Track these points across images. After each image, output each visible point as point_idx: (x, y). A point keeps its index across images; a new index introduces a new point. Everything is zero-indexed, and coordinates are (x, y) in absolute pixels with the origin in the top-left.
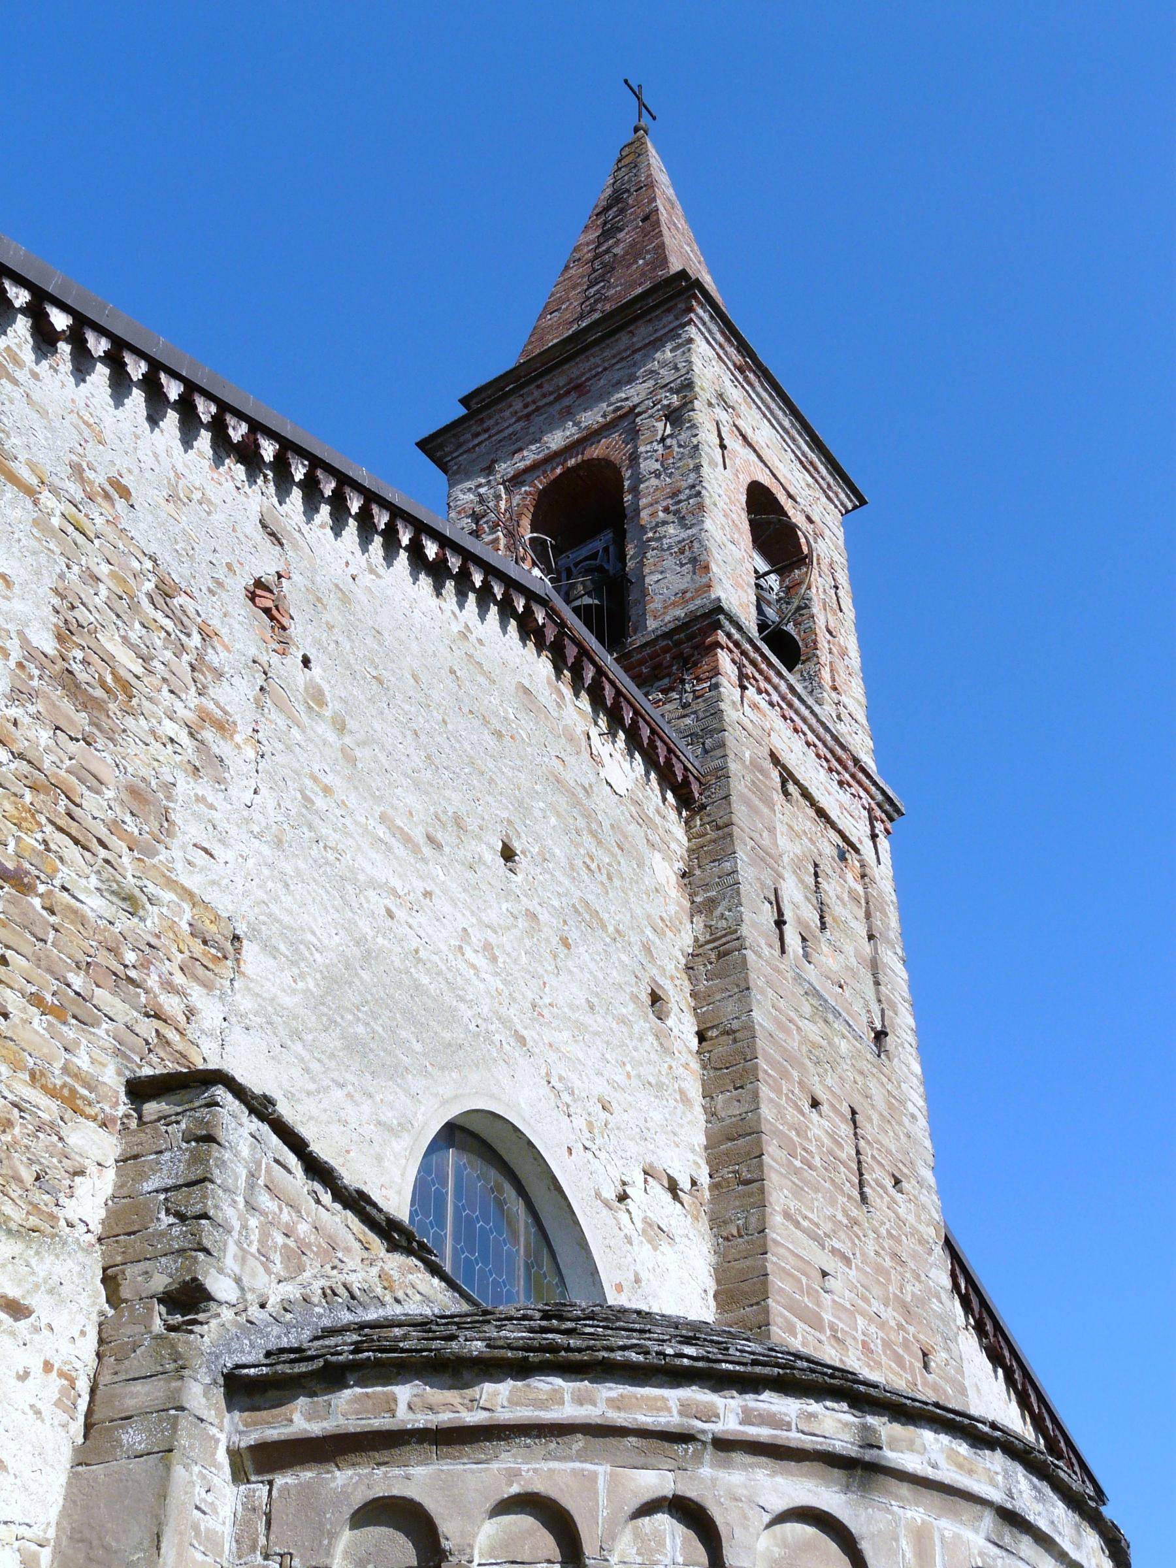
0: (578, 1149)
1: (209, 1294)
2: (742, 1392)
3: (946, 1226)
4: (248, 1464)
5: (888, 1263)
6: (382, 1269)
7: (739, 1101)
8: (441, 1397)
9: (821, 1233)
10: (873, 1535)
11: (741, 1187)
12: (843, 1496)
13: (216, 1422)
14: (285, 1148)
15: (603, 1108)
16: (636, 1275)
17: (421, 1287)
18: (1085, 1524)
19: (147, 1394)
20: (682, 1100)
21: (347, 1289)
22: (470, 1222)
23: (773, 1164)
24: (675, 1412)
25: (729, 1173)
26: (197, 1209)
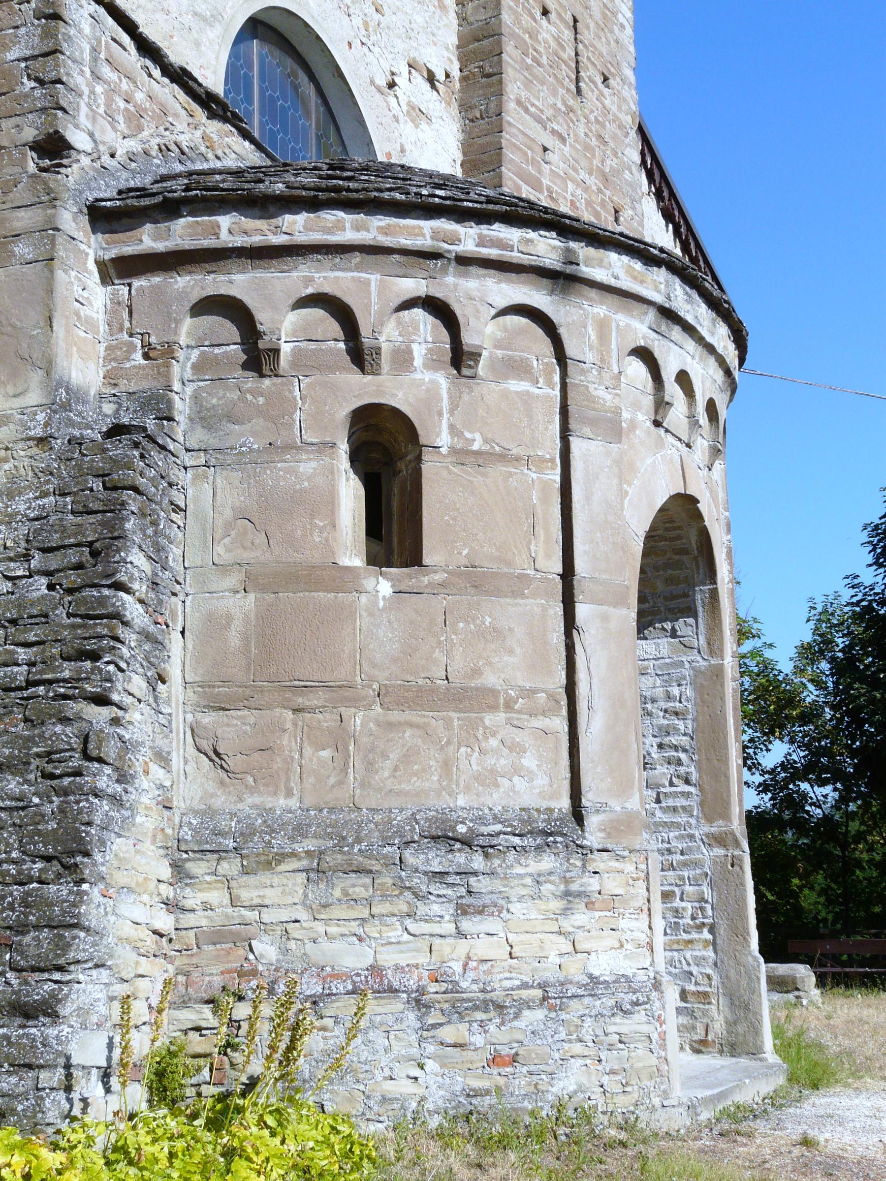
0: (356, 44)
1: (69, 144)
2: (479, 223)
3: (640, 116)
4: (112, 271)
5: (594, 142)
6: (204, 132)
7: (485, 8)
8: (253, 224)
9: (544, 117)
10: (569, 324)
11: (484, 80)
12: (549, 297)
13: (85, 240)
14: (120, 29)
15: (377, 10)
16: (402, 146)
17: (236, 148)
18: (719, 319)
19: (30, 219)
20: (439, 6)
21: (178, 146)
22: (272, 100)
23: (510, 61)
24: (428, 237)
25: (475, 68)
26: (53, 75)
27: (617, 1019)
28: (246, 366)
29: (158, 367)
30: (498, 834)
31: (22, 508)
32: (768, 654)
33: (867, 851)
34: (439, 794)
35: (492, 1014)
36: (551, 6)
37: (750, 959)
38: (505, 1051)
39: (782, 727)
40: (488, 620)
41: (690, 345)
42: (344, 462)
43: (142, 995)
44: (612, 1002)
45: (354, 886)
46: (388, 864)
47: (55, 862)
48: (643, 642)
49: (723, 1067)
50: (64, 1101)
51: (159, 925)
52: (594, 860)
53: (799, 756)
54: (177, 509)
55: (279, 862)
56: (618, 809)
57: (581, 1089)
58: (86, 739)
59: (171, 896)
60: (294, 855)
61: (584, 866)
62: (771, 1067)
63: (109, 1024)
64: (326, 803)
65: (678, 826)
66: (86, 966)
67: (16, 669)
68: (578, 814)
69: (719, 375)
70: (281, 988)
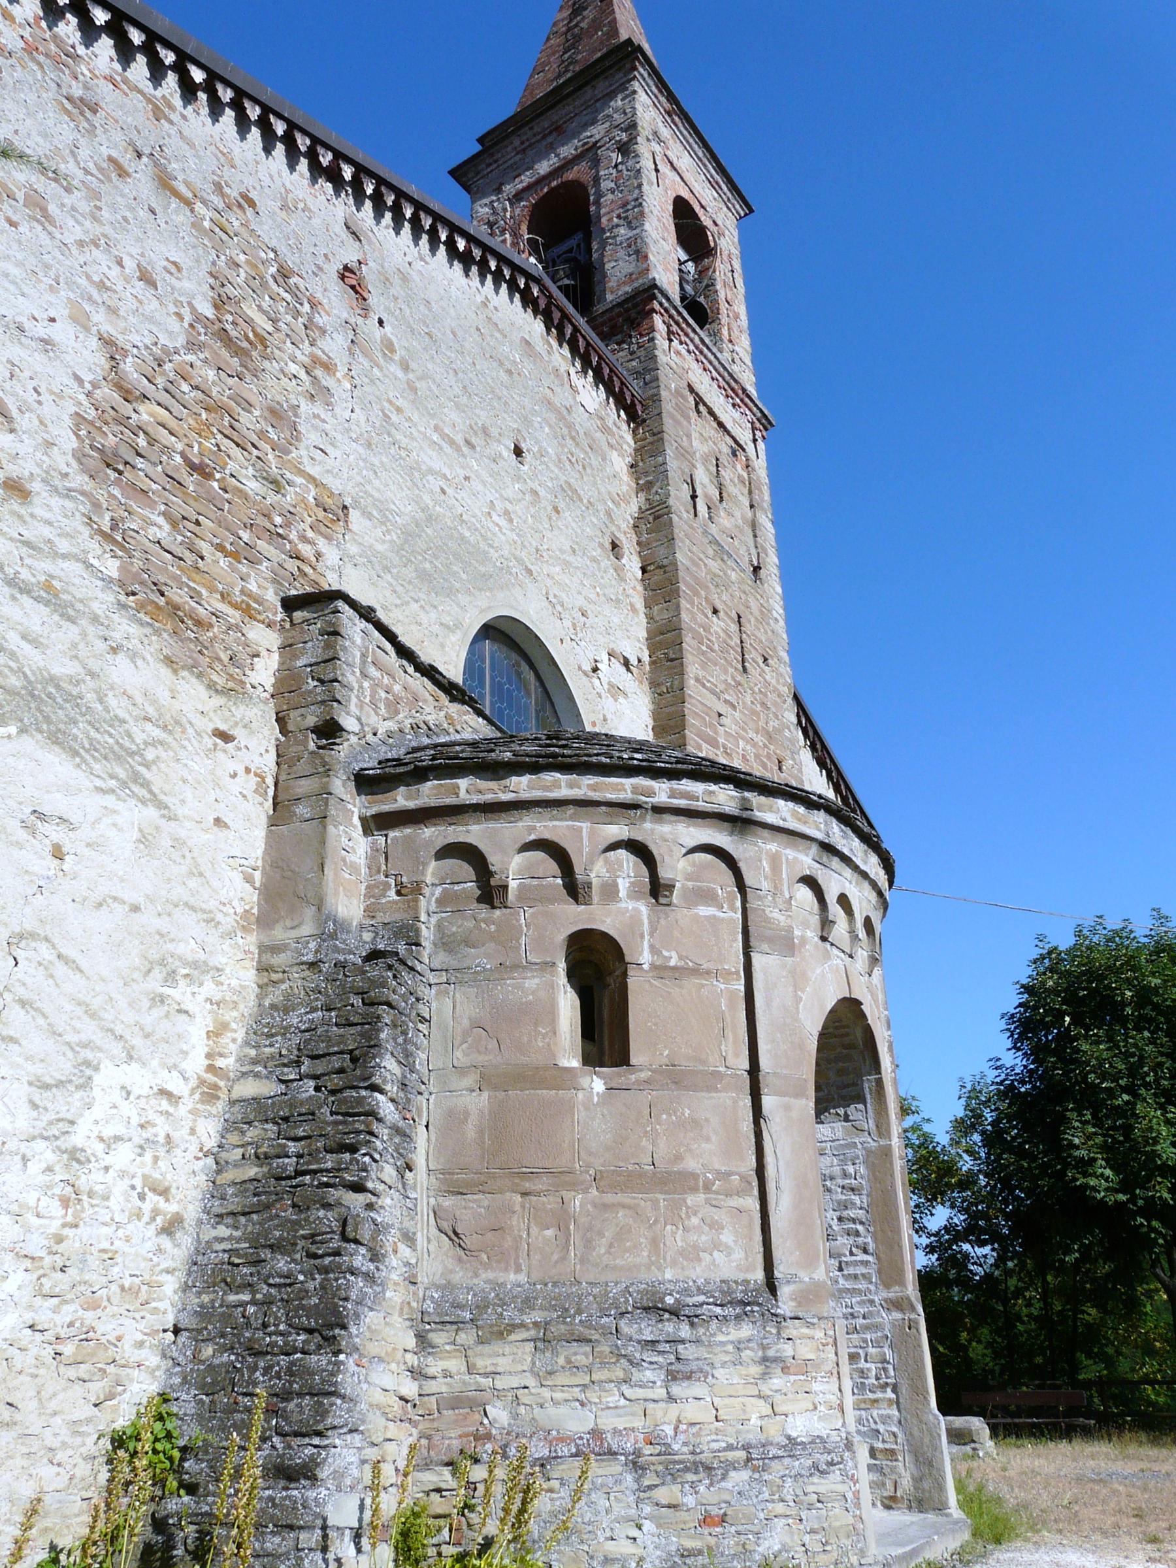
4: (373, 826)
5: (759, 708)
27: (815, 1479)
28: (480, 900)
29: (408, 902)
30: (702, 1305)
31: (295, 1021)
32: (927, 1128)
33: (1026, 1306)
34: (649, 1269)
35: (702, 1475)
36: (719, 606)
37: (931, 1417)
38: (714, 1511)
39: (943, 1194)
40: (687, 1112)
41: (848, 872)
42: (562, 978)
43: (389, 1459)
44: (809, 1462)
45: (576, 1354)
46: (605, 1332)
47: (316, 1334)
48: (820, 1126)
49: (912, 1523)
50: (320, 1561)
51: (404, 1392)
52: (787, 1327)
53: (959, 1219)
54: (423, 1020)
55: (510, 1332)
56: (807, 1279)
57: (785, 1548)
58: (344, 1223)
59: (416, 1364)
60: (523, 1325)
61: (779, 1333)
62: (956, 1522)
63: (360, 1487)
64: (550, 1277)
65: (859, 1292)
66: (342, 1431)
67: (287, 1160)
68: (771, 1285)
69: (873, 896)
70: (512, 1451)
